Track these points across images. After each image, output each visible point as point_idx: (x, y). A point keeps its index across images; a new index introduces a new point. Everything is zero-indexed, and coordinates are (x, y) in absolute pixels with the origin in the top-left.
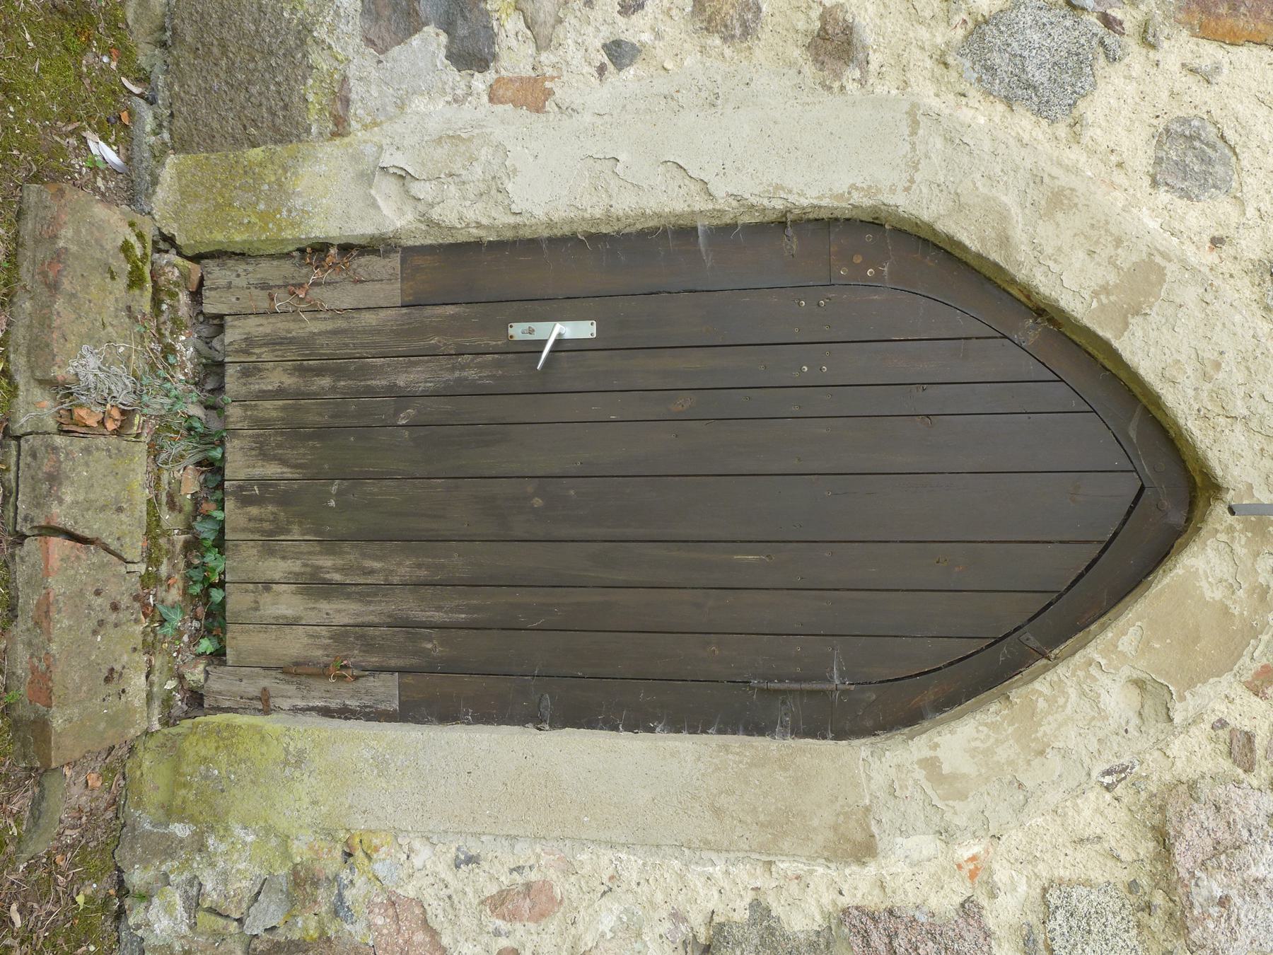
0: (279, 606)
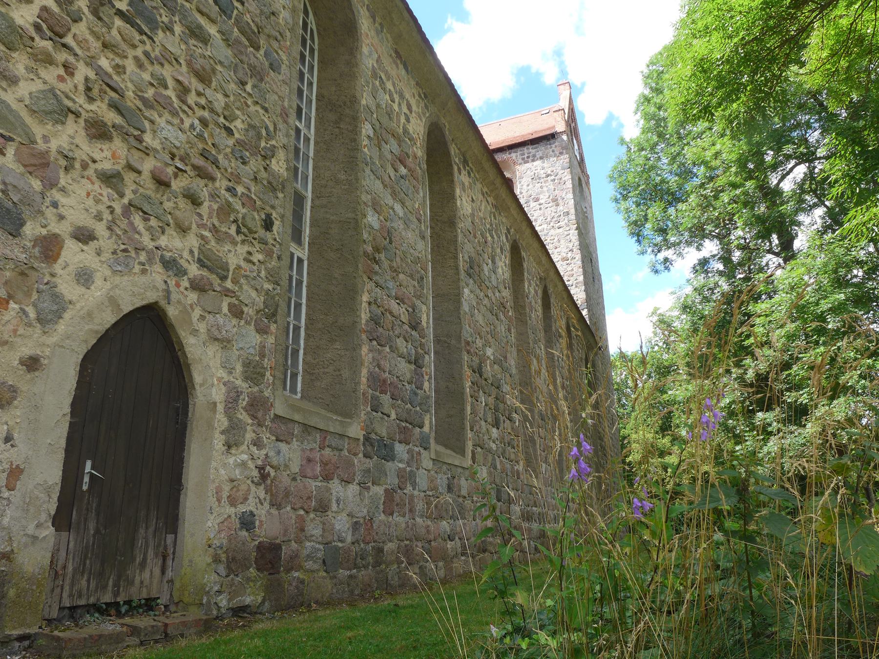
0: (146, 580)
